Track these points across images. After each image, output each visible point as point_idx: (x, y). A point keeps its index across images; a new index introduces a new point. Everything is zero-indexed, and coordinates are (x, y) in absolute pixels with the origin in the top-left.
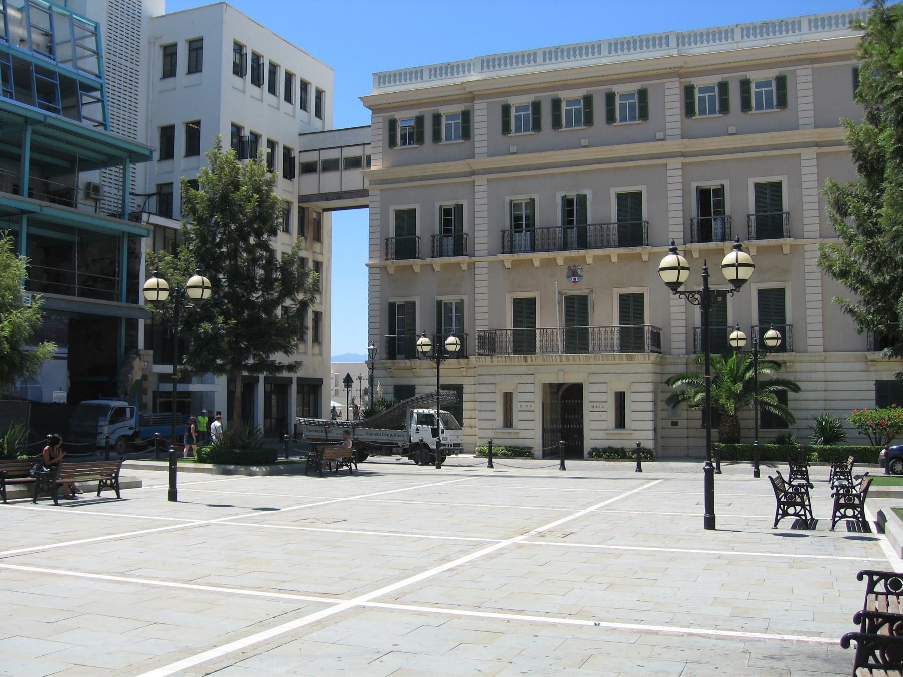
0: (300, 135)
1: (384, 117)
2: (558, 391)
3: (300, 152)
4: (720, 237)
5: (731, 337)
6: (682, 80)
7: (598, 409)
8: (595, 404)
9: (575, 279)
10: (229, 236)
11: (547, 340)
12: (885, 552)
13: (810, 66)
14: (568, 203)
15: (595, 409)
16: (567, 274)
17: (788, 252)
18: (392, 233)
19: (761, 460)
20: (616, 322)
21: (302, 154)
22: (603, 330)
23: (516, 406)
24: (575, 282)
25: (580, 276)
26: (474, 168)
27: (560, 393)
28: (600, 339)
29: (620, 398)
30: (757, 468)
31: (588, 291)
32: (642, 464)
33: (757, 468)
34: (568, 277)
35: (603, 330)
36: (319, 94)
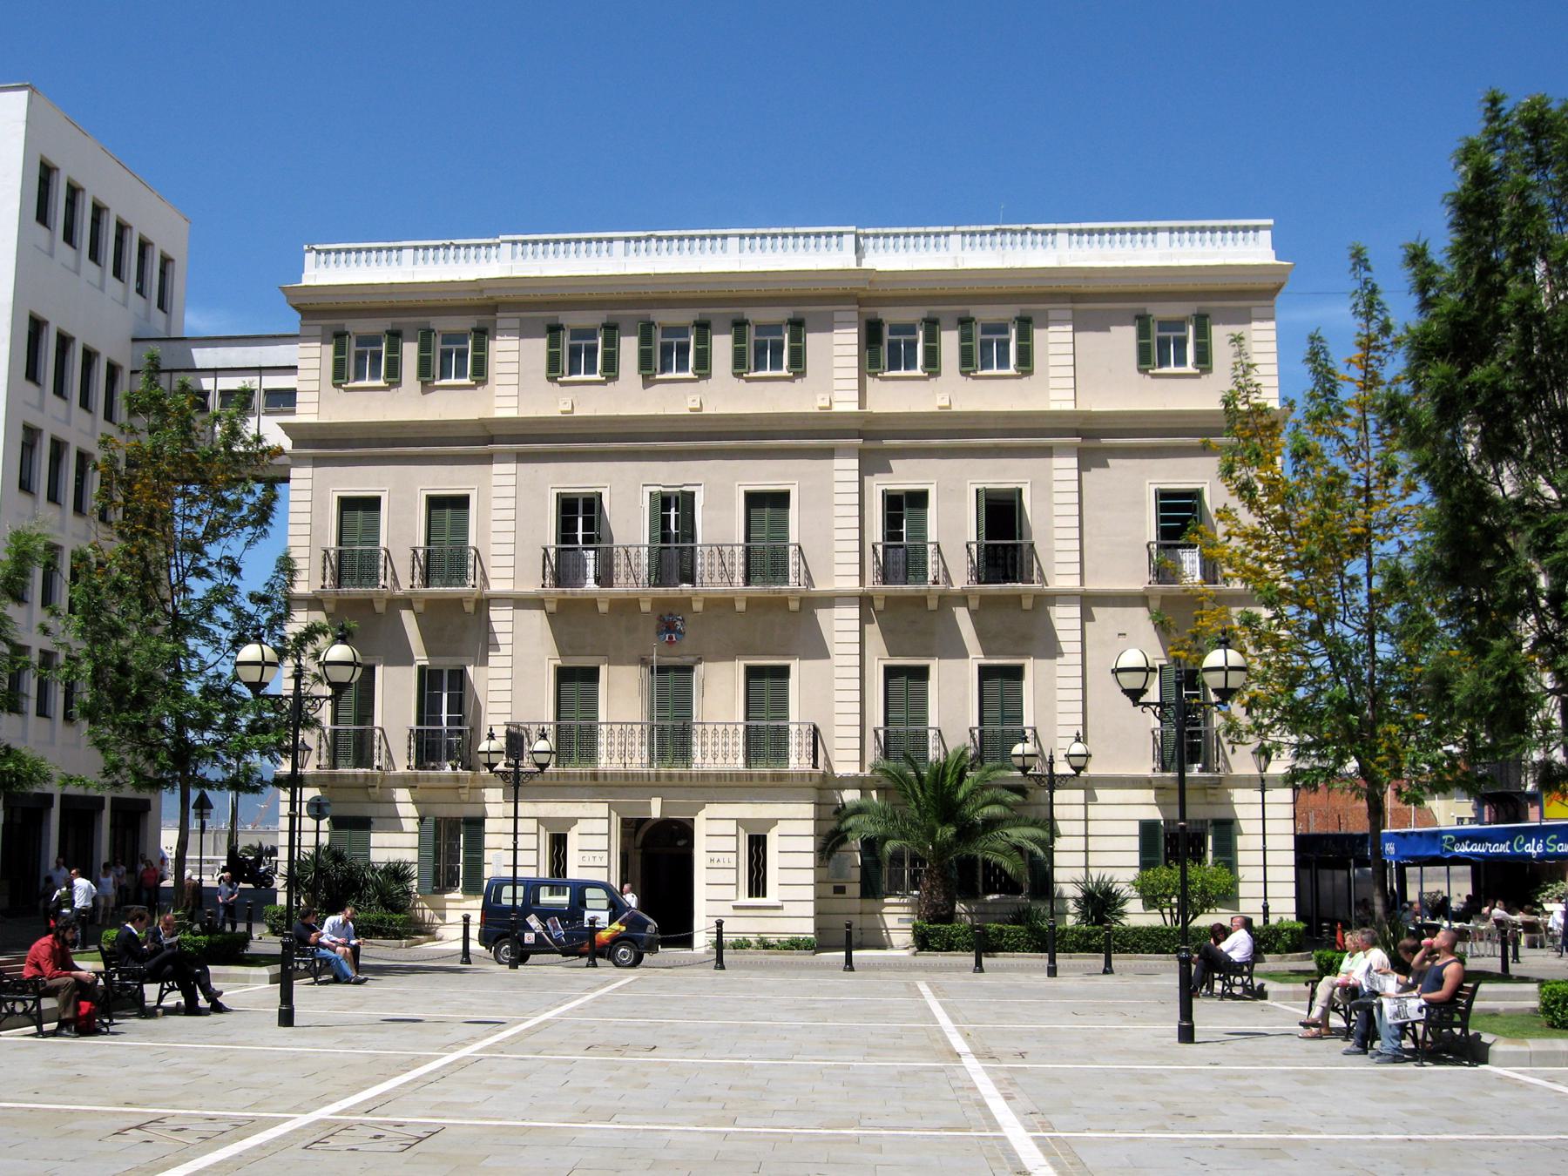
0: (134, 340)
1: (324, 327)
2: (636, 833)
3: (132, 372)
4: (768, 568)
5: (1014, 752)
6: (863, 309)
7: (721, 865)
8: (716, 856)
9: (671, 638)
10: (1541, 629)
11: (632, 744)
12: (999, 1118)
13: (1069, 305)
14: (664, 502)
15: (715, 865)
16: (658, 627)
17: (935, 607)
18: (332, 542)
19: (985, 951)
20: (740, 717)
21: (135, 376)
22: (720, 728)
23: (773, 860)
24: (671, 641)
25: (680, 632)
26: (493, 433)
27: (640, 836)
28: (725, 744)
29: (757, 845)
30: (1052, 960)
31: (692, 659)
32: (854, 953)
33: (1052, 960)
34: (659, 633)
35: (720, 728)
36: (166, 261)
